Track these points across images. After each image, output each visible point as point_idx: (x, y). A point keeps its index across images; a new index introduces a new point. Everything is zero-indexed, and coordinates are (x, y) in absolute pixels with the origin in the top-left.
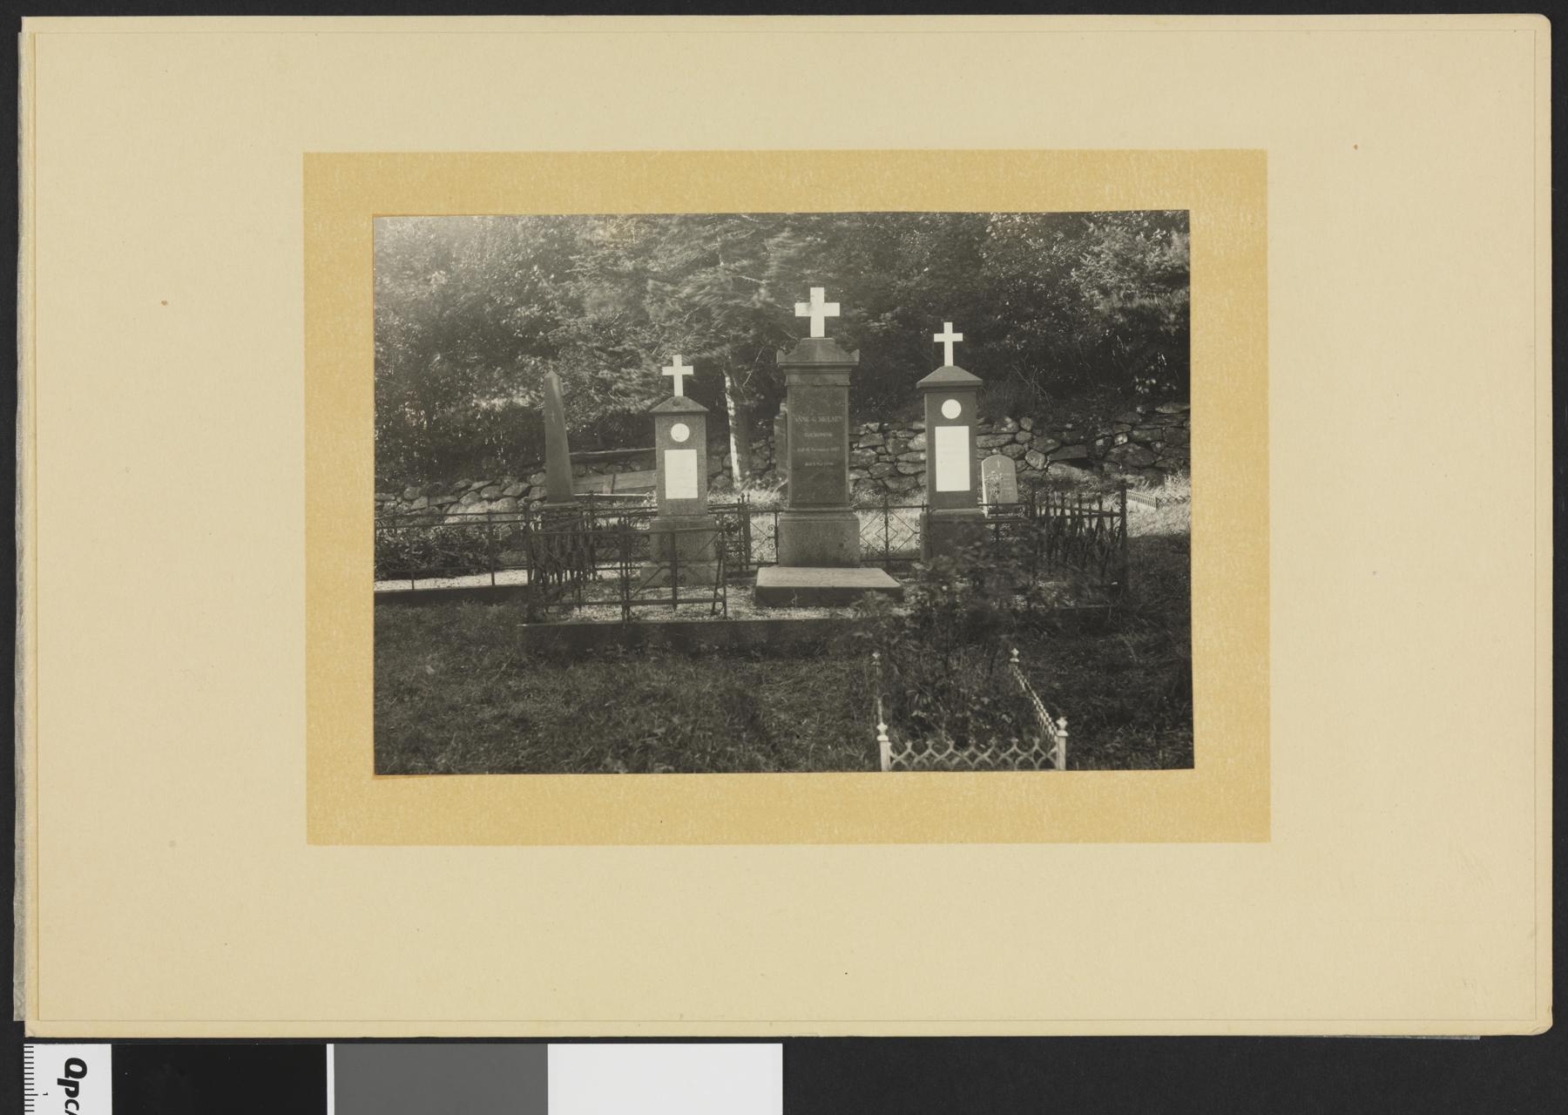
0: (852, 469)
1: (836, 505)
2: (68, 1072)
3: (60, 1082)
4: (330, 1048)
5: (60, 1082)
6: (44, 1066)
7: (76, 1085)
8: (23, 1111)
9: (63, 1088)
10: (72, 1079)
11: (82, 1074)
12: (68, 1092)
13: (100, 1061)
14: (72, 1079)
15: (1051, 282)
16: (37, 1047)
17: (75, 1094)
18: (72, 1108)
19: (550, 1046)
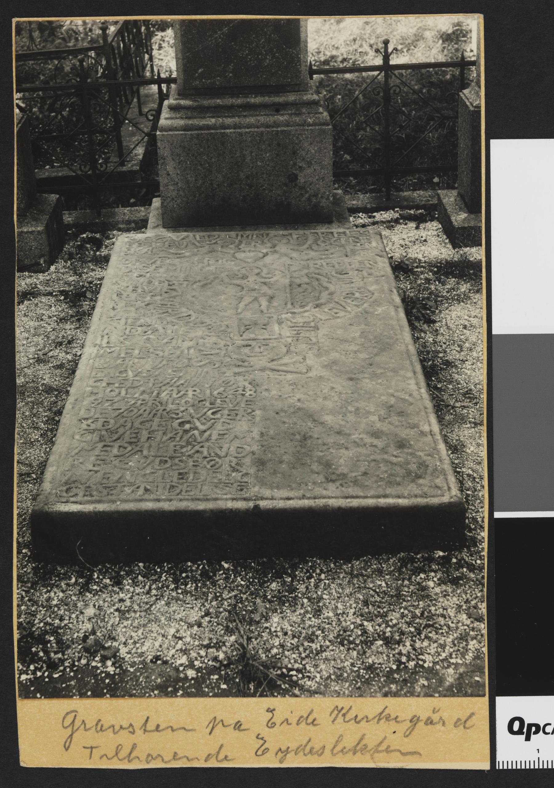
0: (116, 79)
1: (280, 89)
2: (520, 732)
3: (528, 739)
4: (498, 515)
5: (528, 739)
6: (514, 752)
7: (530, 726)
8: (552, 769)
9: (533, 737)
10: (525, 729)
11: (521, 720)
12: (536, 733)
13: (509, 706)
14: (525, 729)
15: (354, 65)
16: (500, 757)
17: (537, 726)
18: (549, 729)
19: (494, 332)
